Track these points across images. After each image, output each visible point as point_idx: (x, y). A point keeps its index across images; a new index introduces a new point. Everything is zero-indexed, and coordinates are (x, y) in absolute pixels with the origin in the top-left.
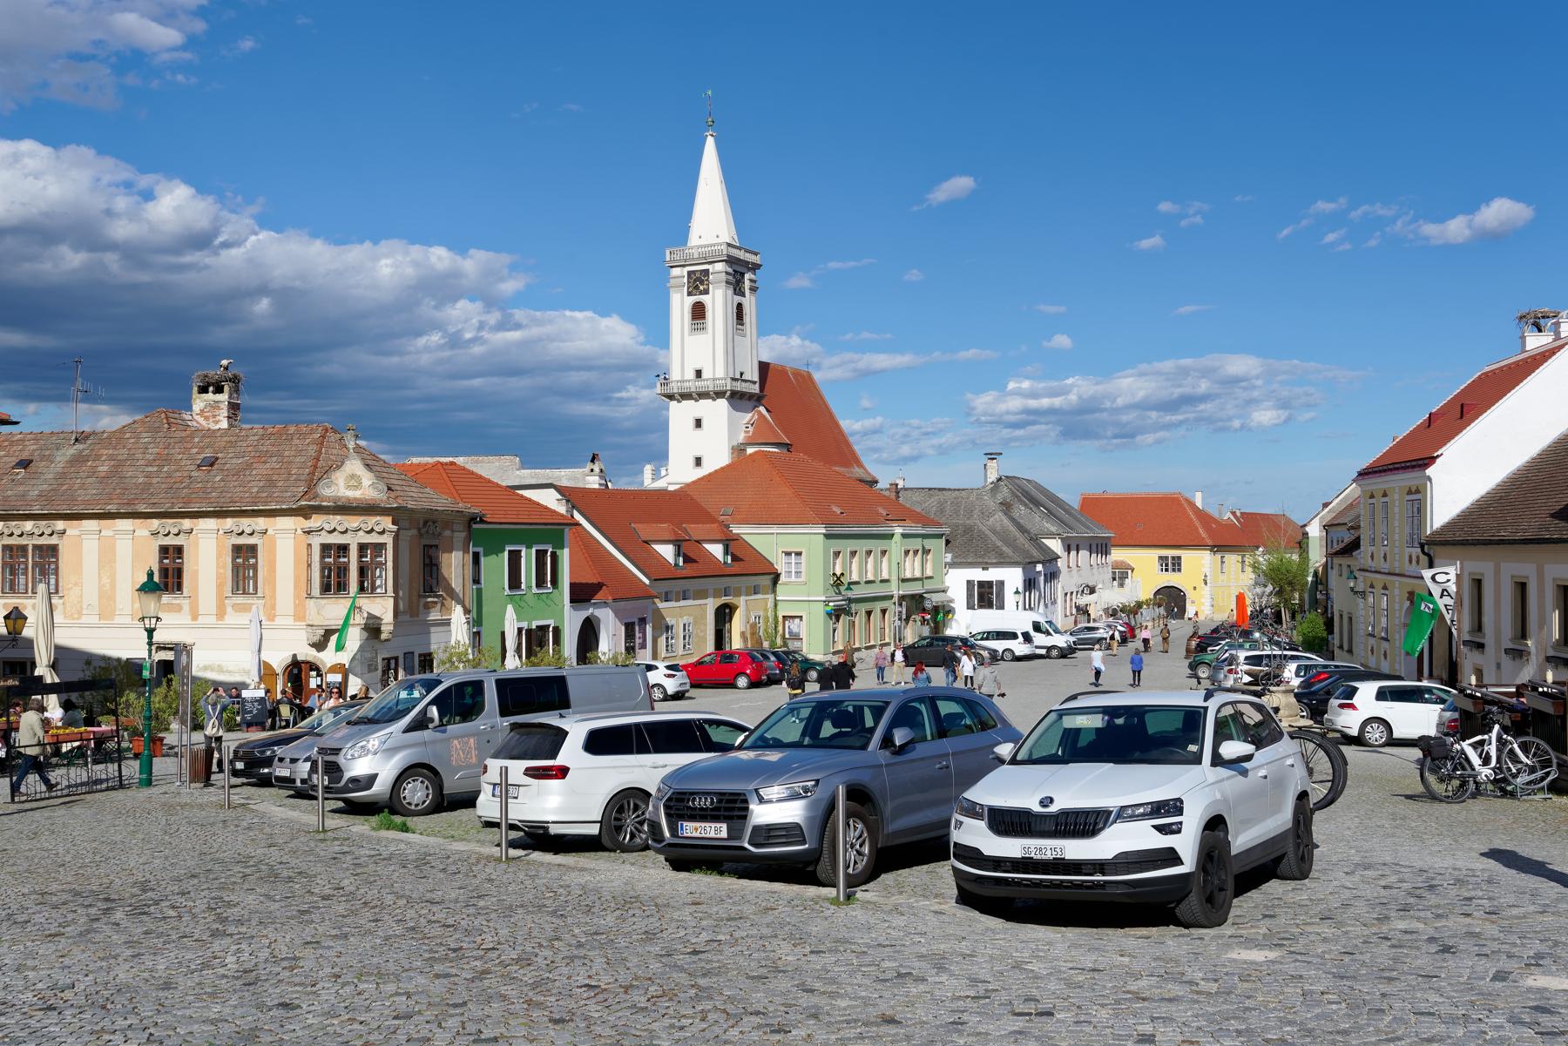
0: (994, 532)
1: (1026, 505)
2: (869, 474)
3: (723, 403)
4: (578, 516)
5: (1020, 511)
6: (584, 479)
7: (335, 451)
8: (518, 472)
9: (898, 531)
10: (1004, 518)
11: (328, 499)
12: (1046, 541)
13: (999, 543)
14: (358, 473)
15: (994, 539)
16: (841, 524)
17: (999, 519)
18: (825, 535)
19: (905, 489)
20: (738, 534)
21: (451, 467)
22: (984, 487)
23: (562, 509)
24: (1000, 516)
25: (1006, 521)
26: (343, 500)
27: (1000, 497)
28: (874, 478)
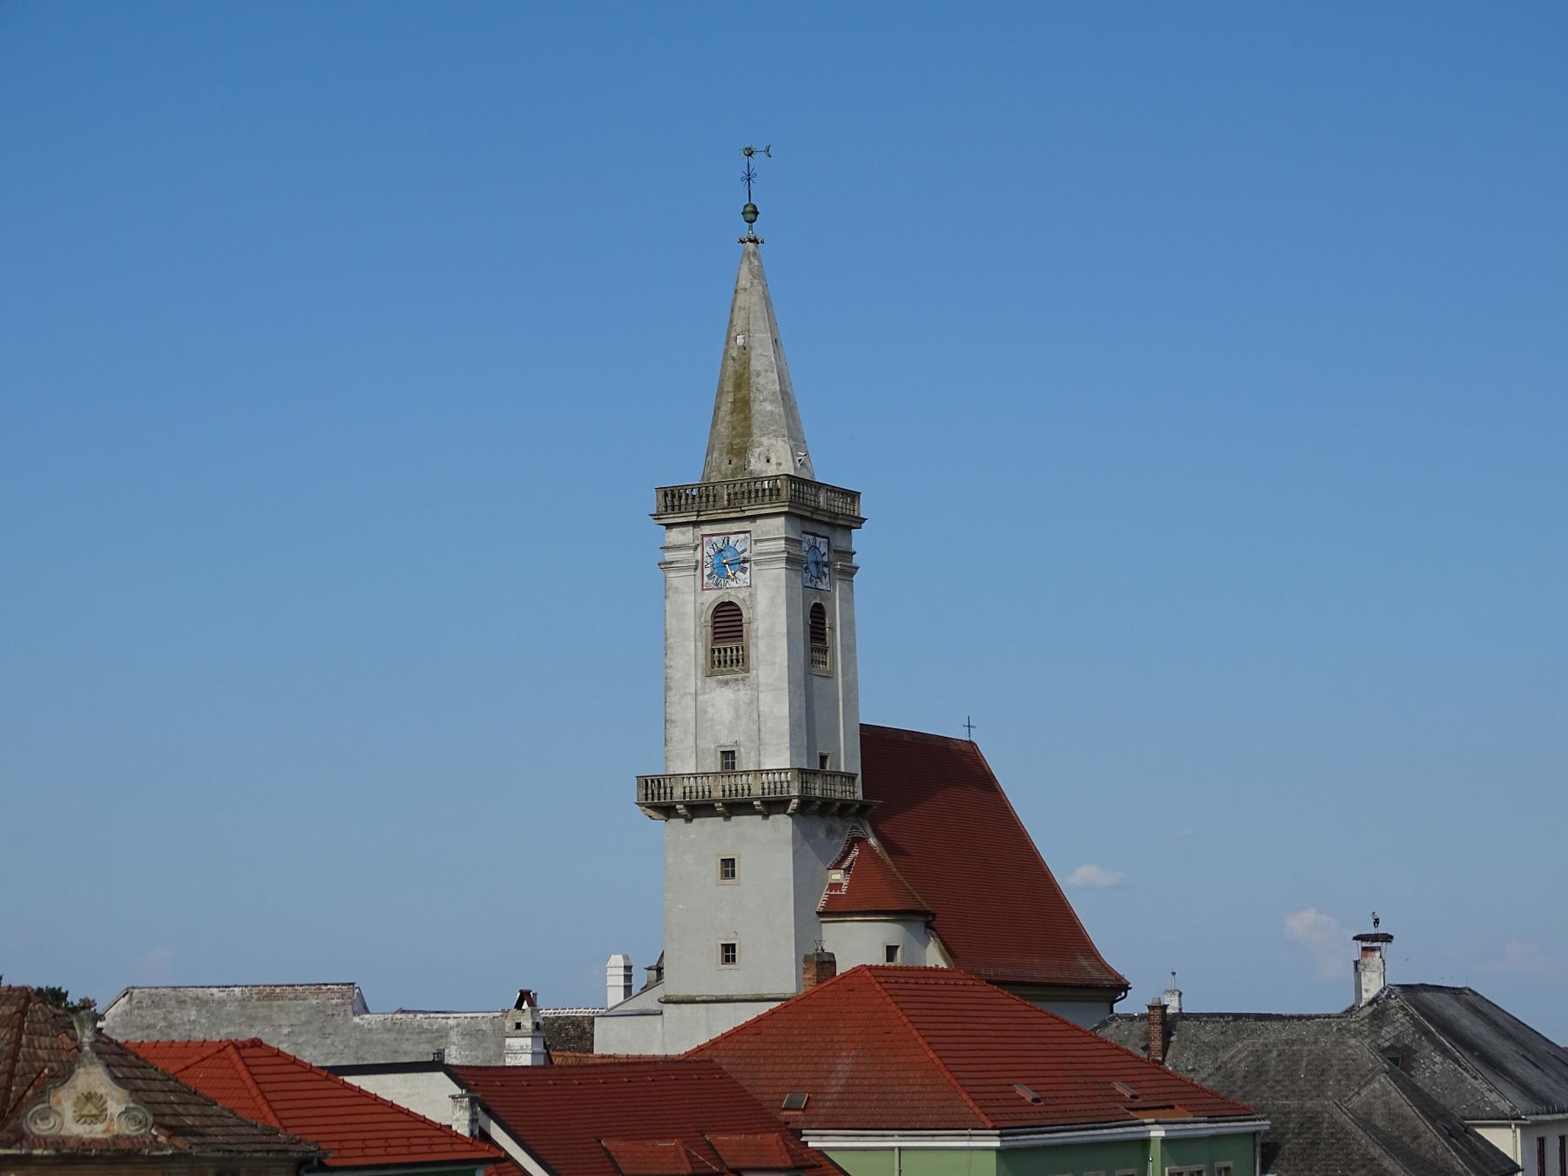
0: (1366, 1123)
1: (1444, 1052)
2: (1109, 970)
3: (782, 826)
4: (497, 1133)
5: (1433, 1067)
6: (501, 1045)
7: (46, 1041)
8: (356, 1019)
9: (1157, 1133)
10: (1392, 1088)
11: (44, 1142)
12: (1485, 1133)
13: (1376, 1151)
14: (102, 1091)
15: (1364, 1140)
16: (1037, 1128)
17: (1382, 1091)
18: (997, 1150)
19: (1182, 1016)
20: (820, 1151)
21: (257, 1051)
22: (1350, 1011)
23: (460, 1123)
24: (1382, 1082)
25: (1397, 1097)
26: (72, 1143)
27: (1387, 1034)
28: (1119, 978)
